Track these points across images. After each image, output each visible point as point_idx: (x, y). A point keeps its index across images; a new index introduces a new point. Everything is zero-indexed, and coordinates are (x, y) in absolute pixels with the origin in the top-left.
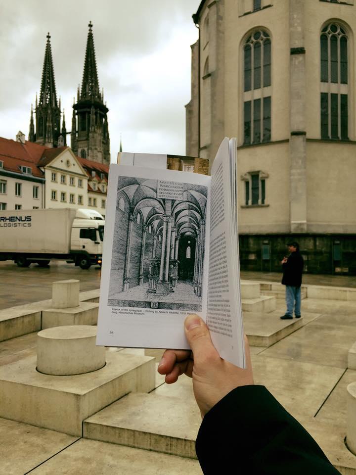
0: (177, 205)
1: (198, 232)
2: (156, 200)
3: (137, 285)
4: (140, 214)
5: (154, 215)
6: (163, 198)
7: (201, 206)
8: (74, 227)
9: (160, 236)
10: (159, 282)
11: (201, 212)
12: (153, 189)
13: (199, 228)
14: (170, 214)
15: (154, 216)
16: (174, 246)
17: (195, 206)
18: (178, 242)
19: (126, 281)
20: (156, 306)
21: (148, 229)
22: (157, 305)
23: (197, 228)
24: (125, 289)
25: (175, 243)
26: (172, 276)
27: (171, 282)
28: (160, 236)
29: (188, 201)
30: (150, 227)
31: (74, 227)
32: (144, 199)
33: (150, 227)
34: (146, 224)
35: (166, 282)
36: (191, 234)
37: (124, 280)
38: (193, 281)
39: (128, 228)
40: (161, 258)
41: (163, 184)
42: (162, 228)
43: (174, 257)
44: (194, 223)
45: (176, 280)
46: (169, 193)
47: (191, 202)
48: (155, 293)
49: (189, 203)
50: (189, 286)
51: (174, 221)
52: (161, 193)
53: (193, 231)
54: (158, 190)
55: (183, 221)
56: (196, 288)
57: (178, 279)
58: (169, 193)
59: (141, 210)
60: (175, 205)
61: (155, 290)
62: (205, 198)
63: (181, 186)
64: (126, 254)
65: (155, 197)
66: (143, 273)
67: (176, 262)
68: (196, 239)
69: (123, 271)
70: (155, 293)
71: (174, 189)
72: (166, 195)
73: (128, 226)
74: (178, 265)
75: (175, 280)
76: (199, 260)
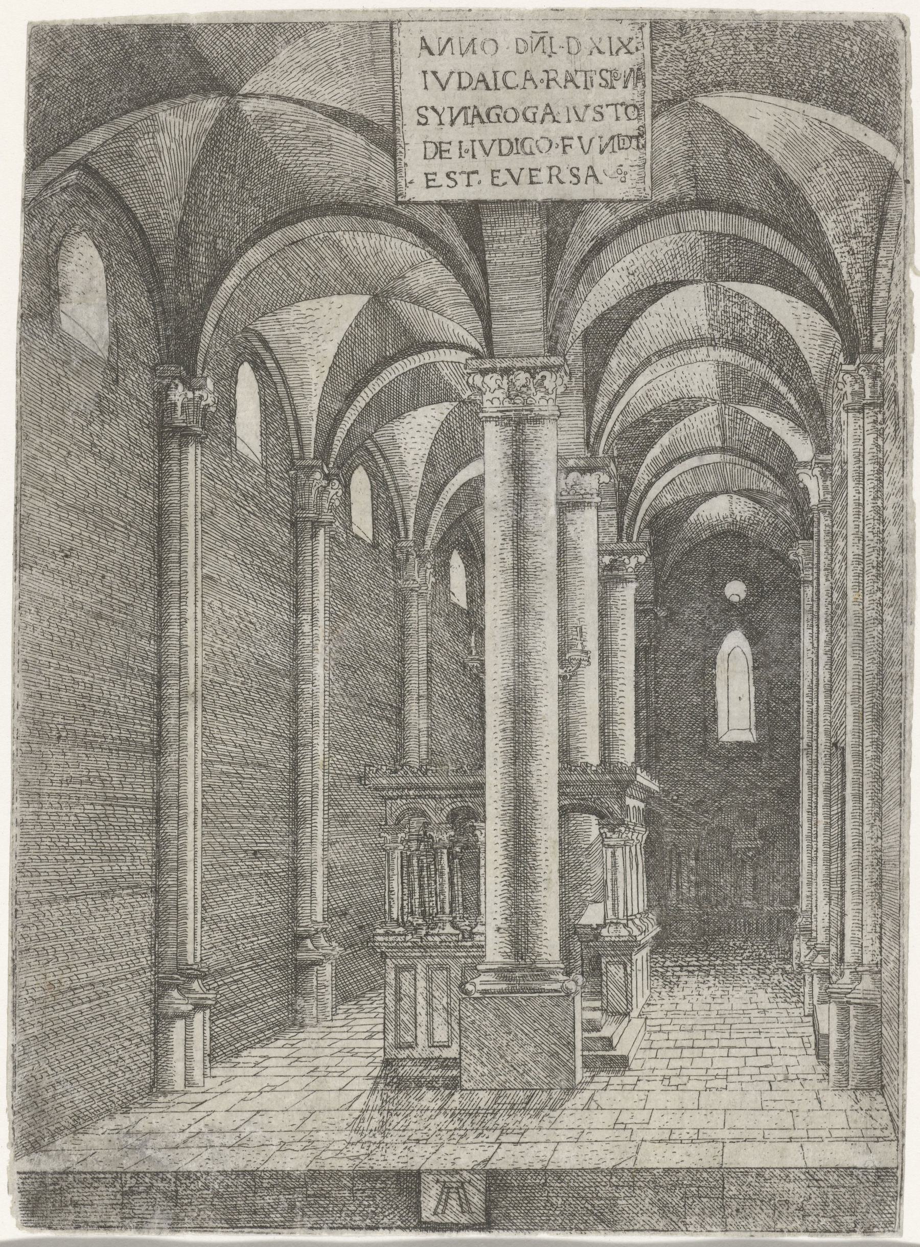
0: (600, 245)
1: (812, 484)
2: (399, 221)
3: (279, 1028)
4: (258, 366)
5: (387, 361)
6: (460, 193)
7: (830, 227)
8: (468, 178)
9: (456, 560)
10: (478, 984)
11: (836, 285)
12: (362, 125)
13: (823, 447)
14: (538, 343)
15: (389, 375)
16: (592, 644)
17: (773, 240)
18: (626, 595)
19: (176, 1001)
20: (465, 1204)
21: (347, 503)
22: (477, 1200)
23: (803, 449)
24: (310, 1008)
25: (603, 614)
26: (593, 915)
27: (594, 969)
28: (456, 560)
29: (705, 204)
30: (360, 481)
31: (468, 178)
32: (279, 223)
33: (360, 481)
34: (323, 453)
35: (544, 974)
36: (743, 509)
37: (160, 988)
38: (800, 947)
39: (161, 513)
40: (480, 764)
41: (444, 64)
42: (475, 486)
43: (607, 742)
44: (776, 404)
45: (641, 957)
46: (517, 145)
47: (736, 209)
48: (454, 1085)
49: (716, 221)
50: (762, 997)
51: (575, 403)
52: (440, 151)
53: (767, 484)
54: (409, 118)
55: (659, 397)
56: (828, 1019)
57: (660, 945)
58: (517, 145)
59: (269, 328)
60: (577, 247)
61: (444, 1063)
62: (876, 142)
63: (624, 62)
64: (158, 749)
65: (385, 198)
66: (329, 913)
67: (623, 786)
68: (798, 553)
69: (146, 905)
70: (454, 1085)
71: (560, 97)
72: (482, 164)
73: (160, 492)
74: (649, 818)
75: (626, 949)
76: (837, 747)
